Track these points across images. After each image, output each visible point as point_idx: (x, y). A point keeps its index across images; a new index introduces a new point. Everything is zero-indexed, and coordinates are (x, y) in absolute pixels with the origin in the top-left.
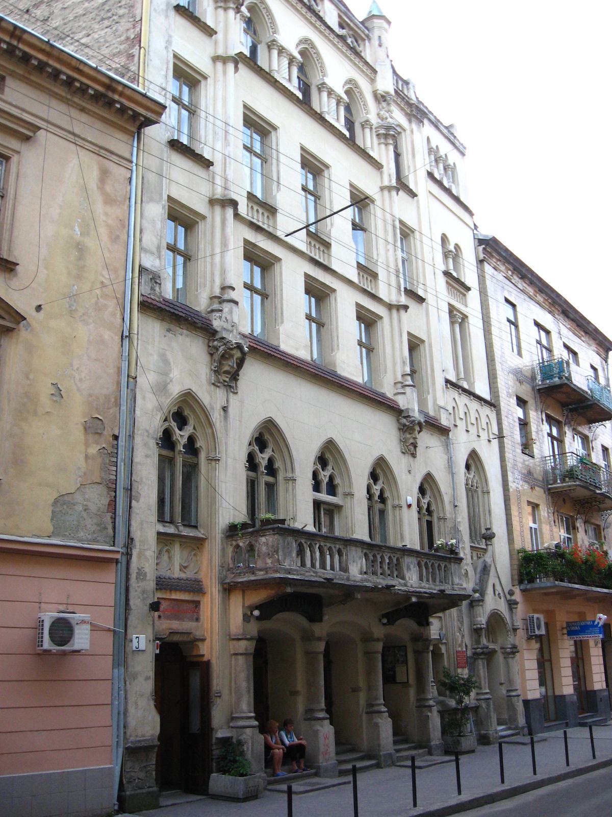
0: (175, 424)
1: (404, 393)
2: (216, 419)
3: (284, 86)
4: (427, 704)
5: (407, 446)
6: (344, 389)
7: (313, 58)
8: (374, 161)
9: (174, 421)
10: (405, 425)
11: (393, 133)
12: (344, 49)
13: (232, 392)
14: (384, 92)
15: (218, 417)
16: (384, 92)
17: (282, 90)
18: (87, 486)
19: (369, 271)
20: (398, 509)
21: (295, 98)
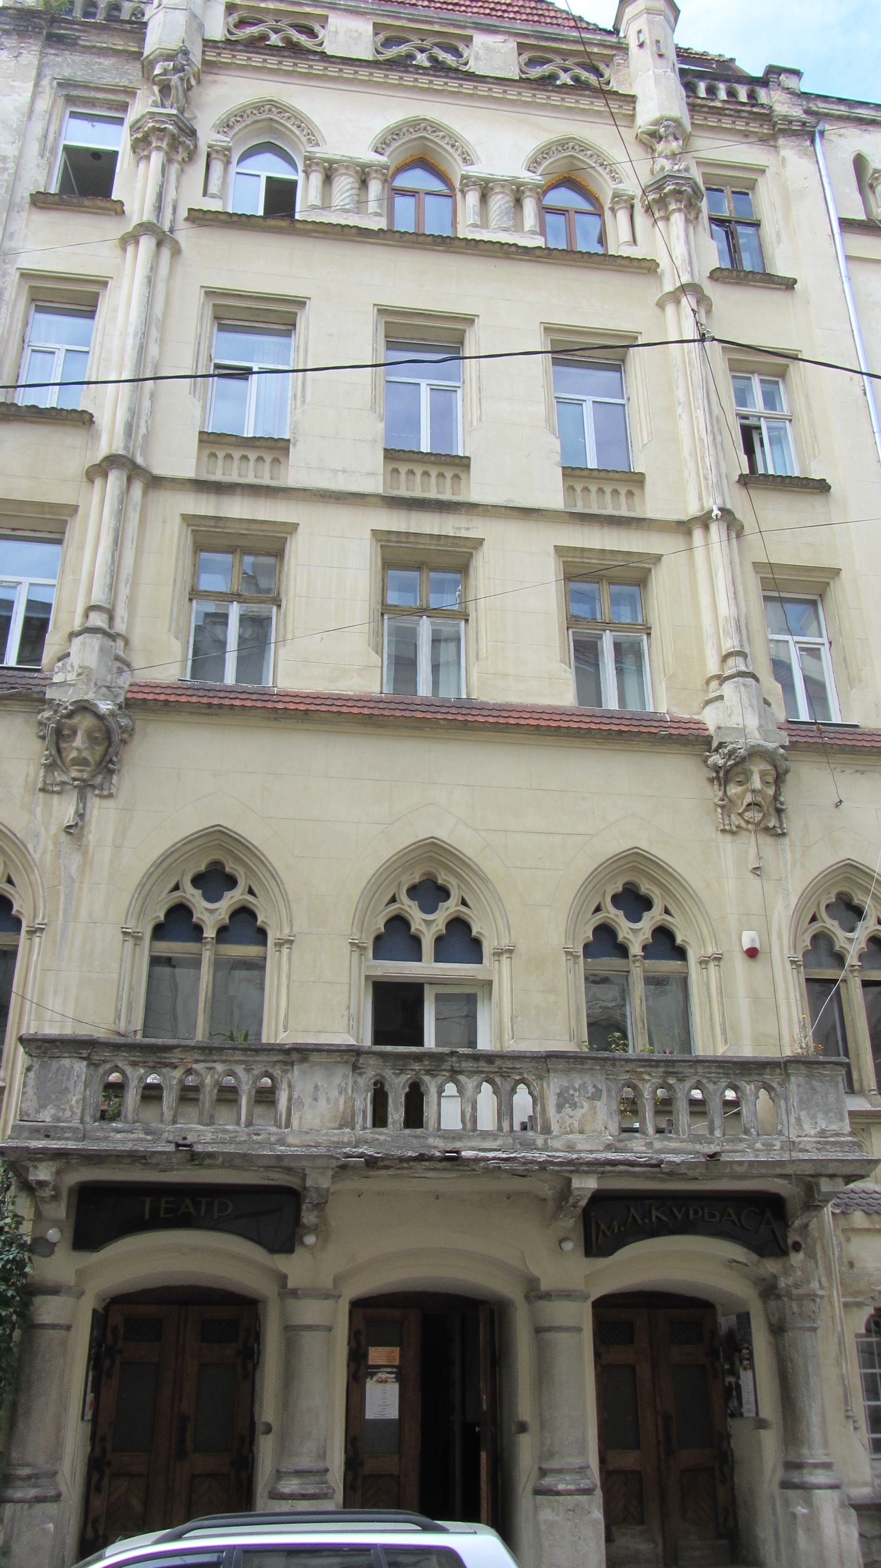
0: (836, 923)
1: (721, 697)
2: (44, 853)
3: (313, 222)
4: (796, 1480)
5: (740, 814)
6: (474, 729)
7: (443, 148)
8: (623, 262)
9: (833, 917)
10: (717, 769)
11: (672, 187)
12: (272, 62)
13: (96, 795)
14: (652, 125)
15: (51, 847)
16: (652, 125)
17: (316, 231)
18: (312, 1034)
19: (611, 475)
20: (712, 965)
21: (354, 231)
